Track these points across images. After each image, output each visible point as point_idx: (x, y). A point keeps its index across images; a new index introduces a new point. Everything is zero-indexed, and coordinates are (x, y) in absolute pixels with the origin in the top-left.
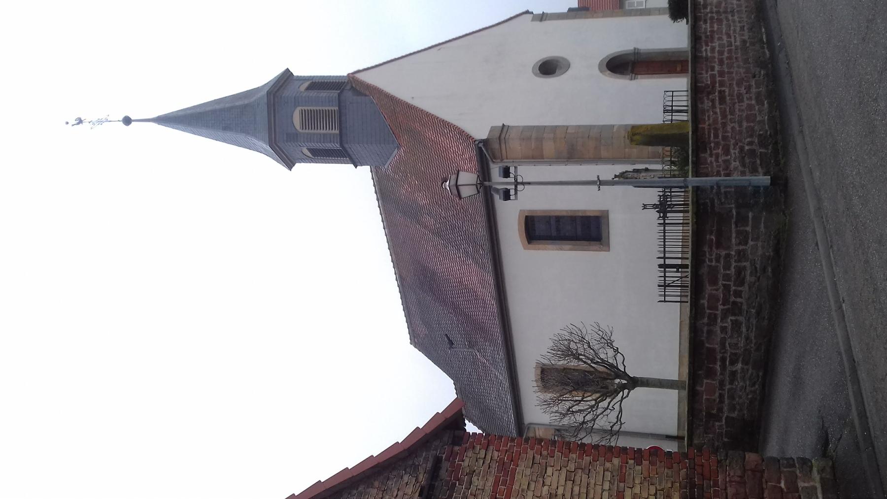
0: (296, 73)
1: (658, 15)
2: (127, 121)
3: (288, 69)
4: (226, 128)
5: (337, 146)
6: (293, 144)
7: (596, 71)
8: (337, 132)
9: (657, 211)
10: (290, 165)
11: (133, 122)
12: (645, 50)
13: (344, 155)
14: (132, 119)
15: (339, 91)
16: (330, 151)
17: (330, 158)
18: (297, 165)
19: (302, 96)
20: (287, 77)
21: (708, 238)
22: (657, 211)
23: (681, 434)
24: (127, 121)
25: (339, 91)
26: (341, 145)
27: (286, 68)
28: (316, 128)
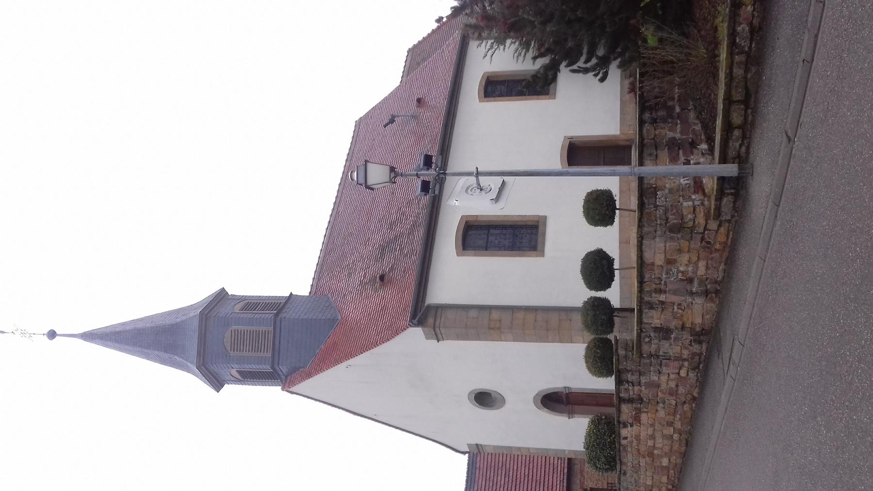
0: (230, 292)
1: (531, 448)
2: (52, 335)
3: (223, 288)
4: (148, 347)
5: (267, 368)
6: (225, 365)
7: (434, 21)
8: (269, 354)
9: (594, 75)
10: (217, 384)
11: (57, 337)
12: (576, 389)
13: (275, 377)
14: (57, 333)
15: (275, 312)
16: (264, 373)
17: (261, 380)
18: (226, 386)
19: (218, 316)
20: (221, 296)
21: (469, 10)
22: (594, 75)
23: (627, 305)
24: (52, 335)
25: (275, 312)
26: (273, 367)
27: (221, 287)
28: (265, 351)
